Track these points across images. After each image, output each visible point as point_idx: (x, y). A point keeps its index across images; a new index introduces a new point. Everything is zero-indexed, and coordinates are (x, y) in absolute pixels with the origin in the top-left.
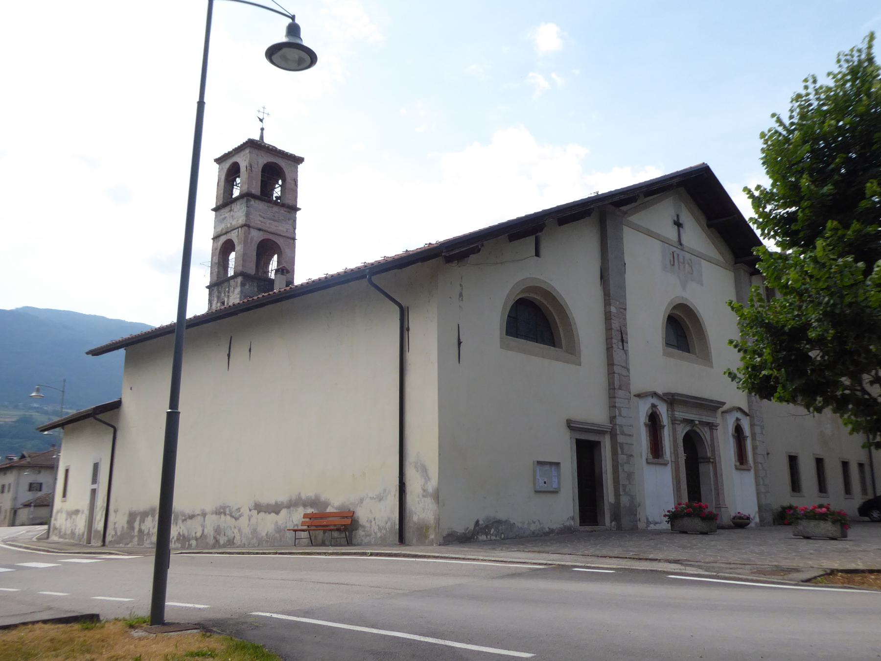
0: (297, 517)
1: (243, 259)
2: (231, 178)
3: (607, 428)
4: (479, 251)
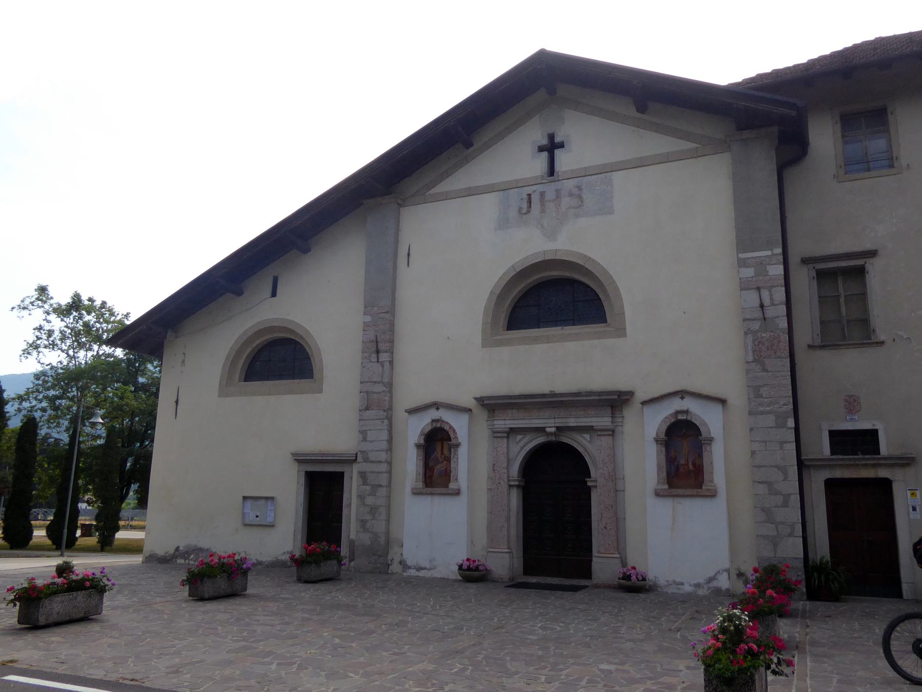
3: (350, 457)
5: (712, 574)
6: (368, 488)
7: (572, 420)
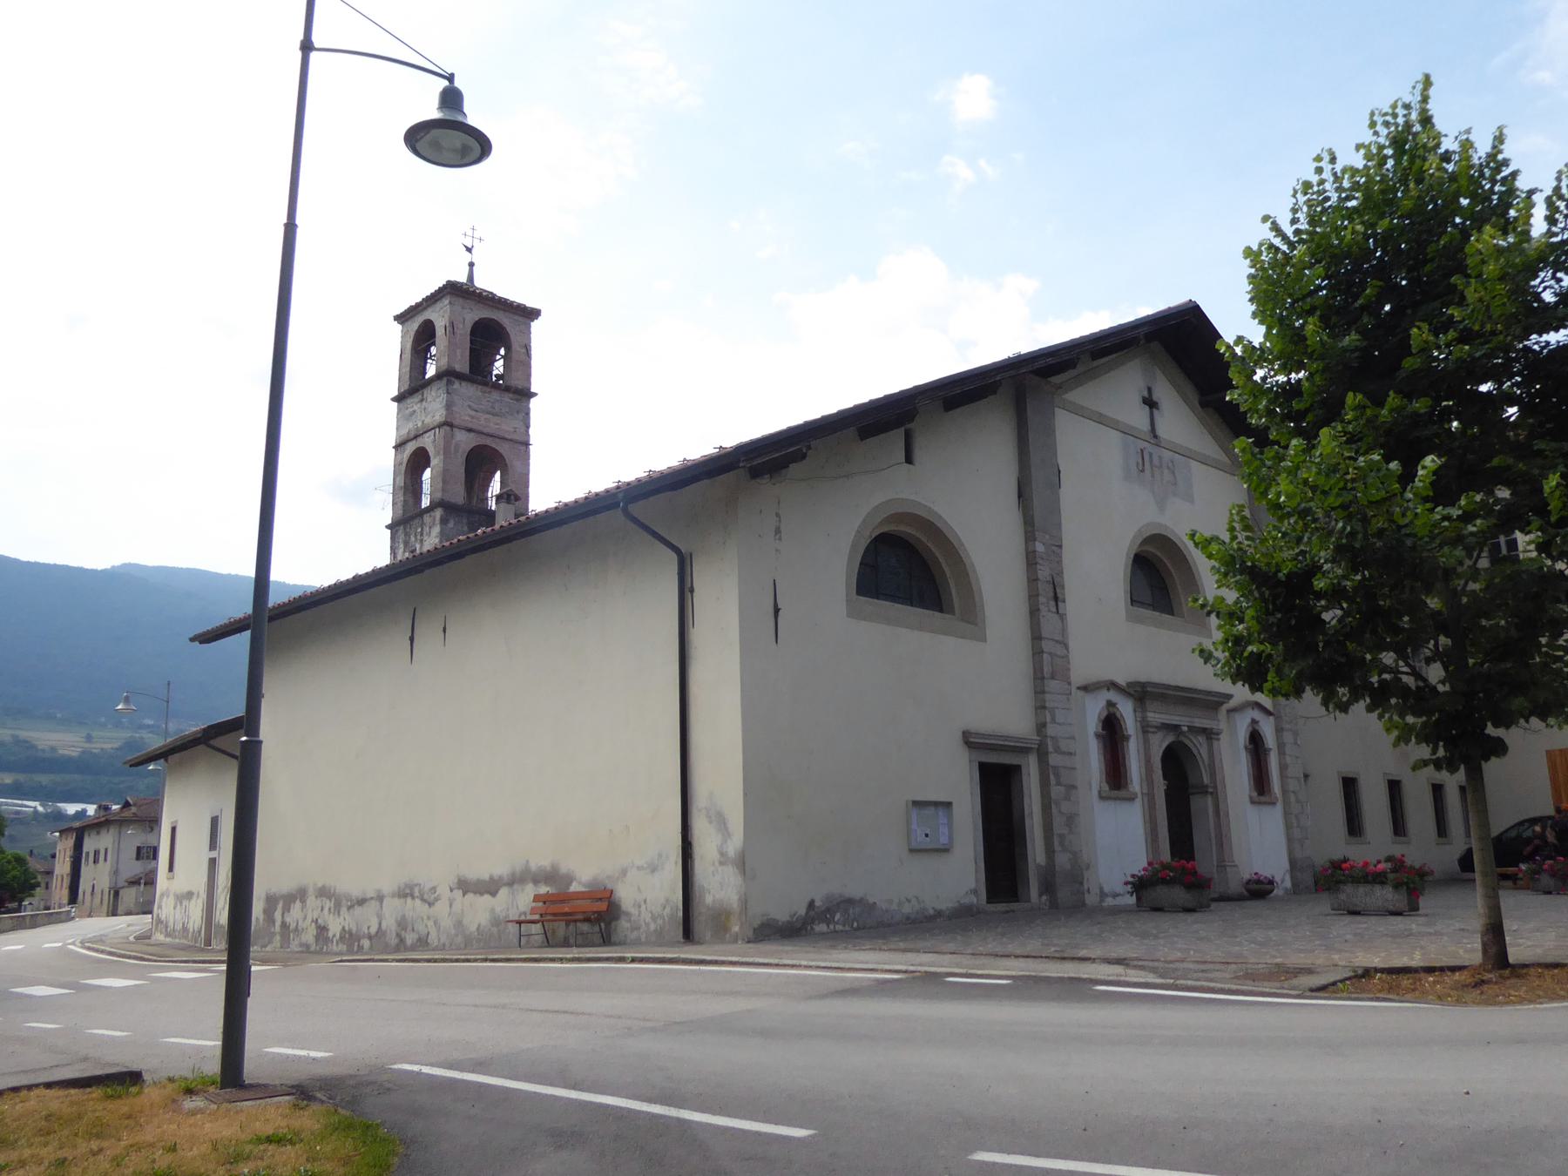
0: (523, 900)
1: (444, 478)
2: (423, 346)
4: (804, 456)
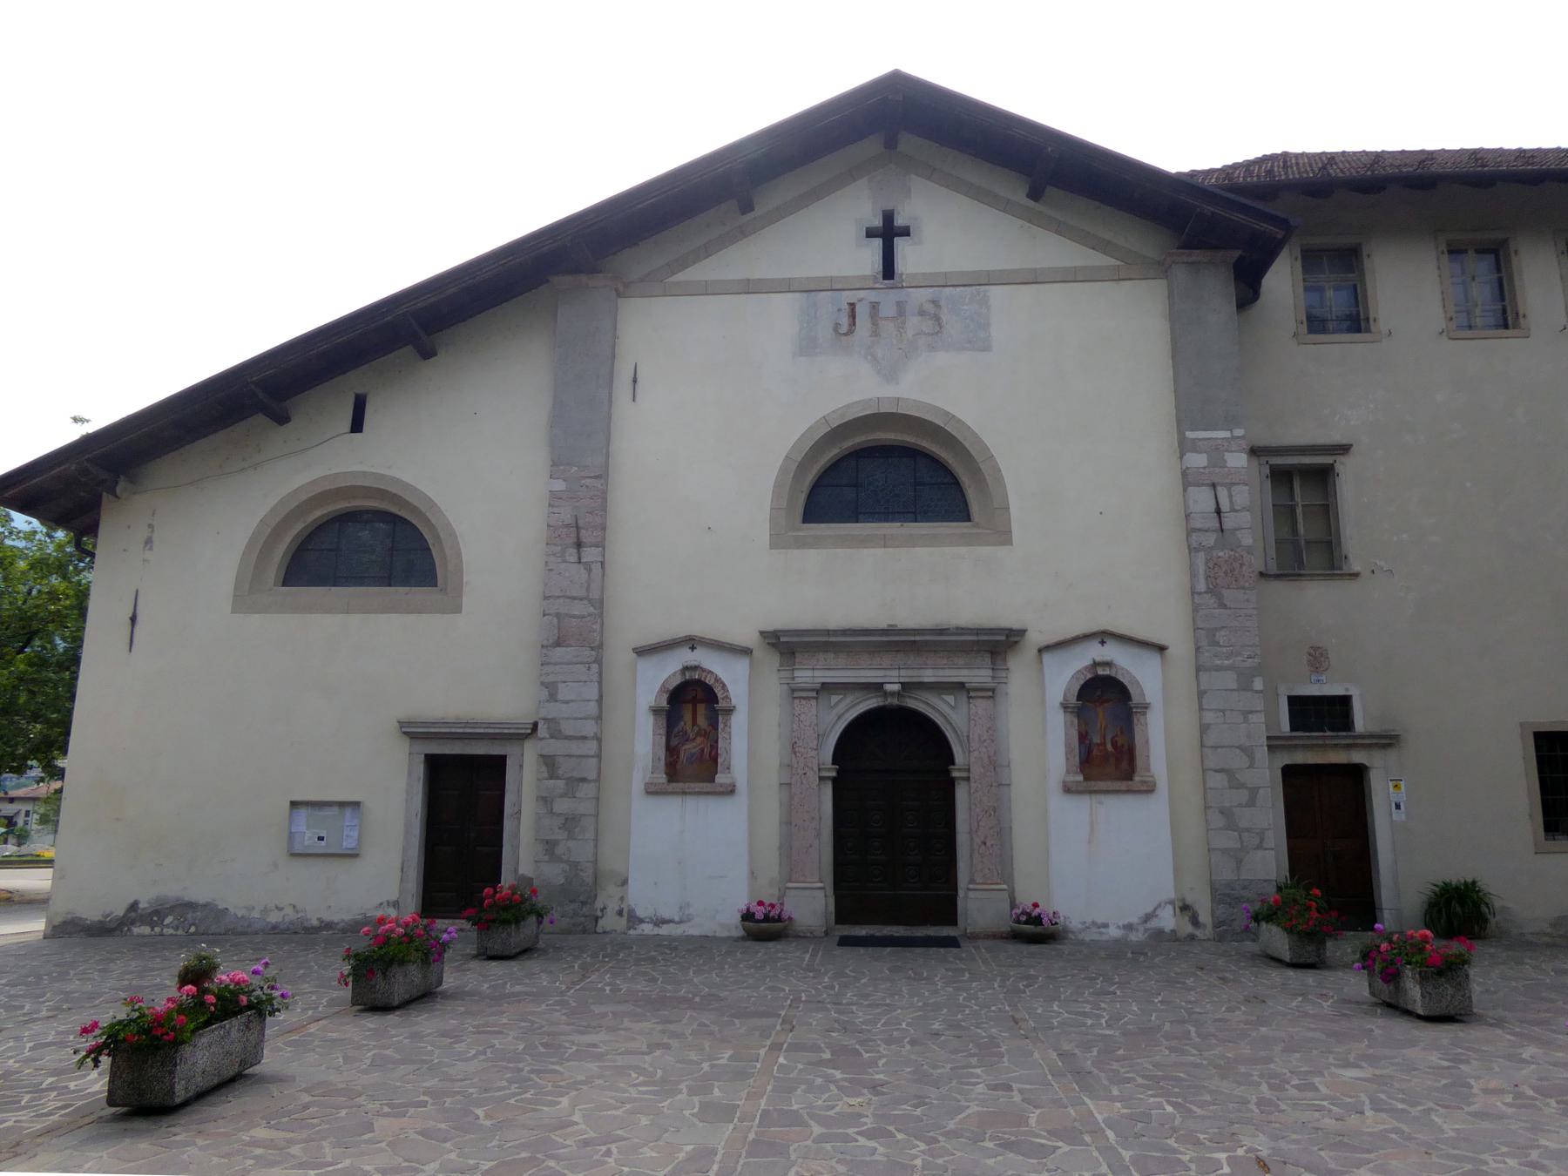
3: (522, 728)
5: (1149, 909)
6: (561, 783)
7: (929, 672)
